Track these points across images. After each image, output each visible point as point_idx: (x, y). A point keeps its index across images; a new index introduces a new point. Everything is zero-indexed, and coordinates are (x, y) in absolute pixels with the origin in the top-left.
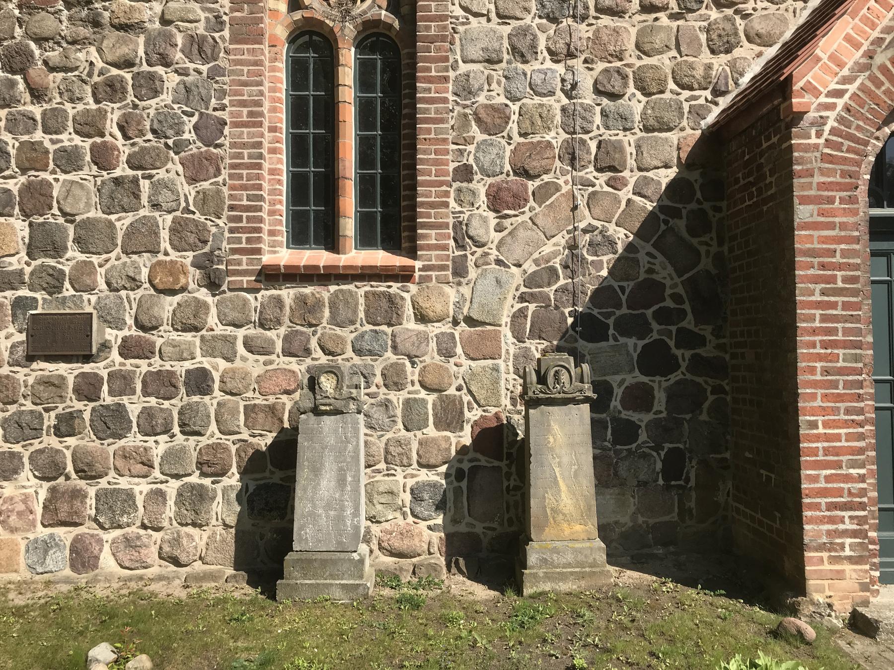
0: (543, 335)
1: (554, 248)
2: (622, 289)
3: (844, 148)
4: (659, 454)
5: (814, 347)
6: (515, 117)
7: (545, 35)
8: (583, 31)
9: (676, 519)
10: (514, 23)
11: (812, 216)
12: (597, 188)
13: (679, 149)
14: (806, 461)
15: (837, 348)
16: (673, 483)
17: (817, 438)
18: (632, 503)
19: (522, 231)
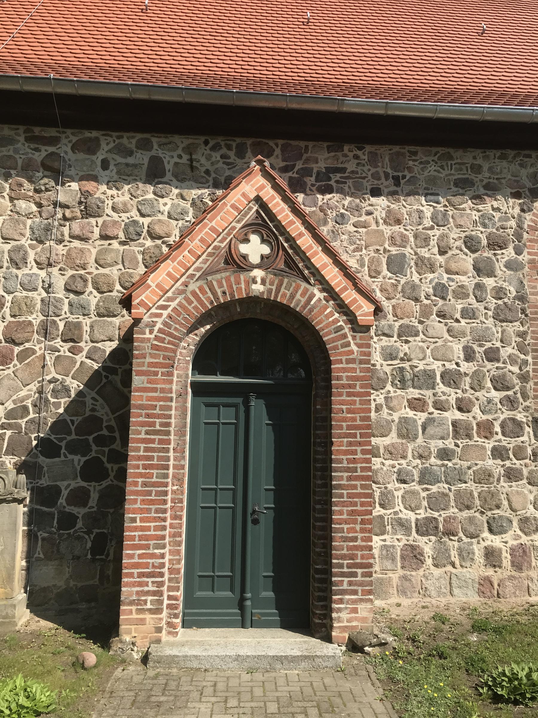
0: (15, 453)
1: (28, 393)
2: (72, 422)
3: (166, 342)
4: (90, 537)
5: (138, 468)
6: (8, 304)
7: (34, 252)
8: (61, 250)
9: (97, 583)
10: (13, 243)
11: (143, 383)
12: (62, 353)
13: (119, 329)
14: (127, 544)
15: (153, 469)
16: (98, 557)
17: (136, 529)
18: (67, 571)
19: (6, 380)
